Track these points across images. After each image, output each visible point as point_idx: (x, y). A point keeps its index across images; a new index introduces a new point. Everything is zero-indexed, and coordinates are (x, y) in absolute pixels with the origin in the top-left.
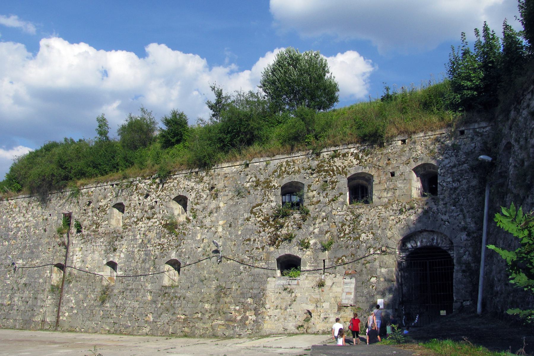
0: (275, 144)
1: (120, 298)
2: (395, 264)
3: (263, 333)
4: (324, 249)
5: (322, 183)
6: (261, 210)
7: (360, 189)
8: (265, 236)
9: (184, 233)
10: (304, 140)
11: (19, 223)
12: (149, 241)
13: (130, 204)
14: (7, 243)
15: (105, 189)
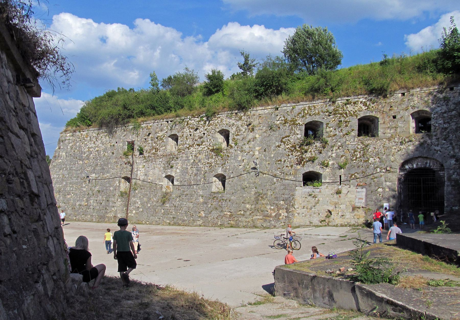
0: (297, 94)
1: (178, 200)
2: (397, 179)
3: (293, 225)
4: (341, 168)
5: (338, 122)
6: (289, 140)
7: (367, 127)
8: (294, 157)
9: (228, 155)
10: (322, 92)
11: (91, 148)
12: (199, 161)
13: (183, 135)
14: (81, 162)
15: (162, 125)
